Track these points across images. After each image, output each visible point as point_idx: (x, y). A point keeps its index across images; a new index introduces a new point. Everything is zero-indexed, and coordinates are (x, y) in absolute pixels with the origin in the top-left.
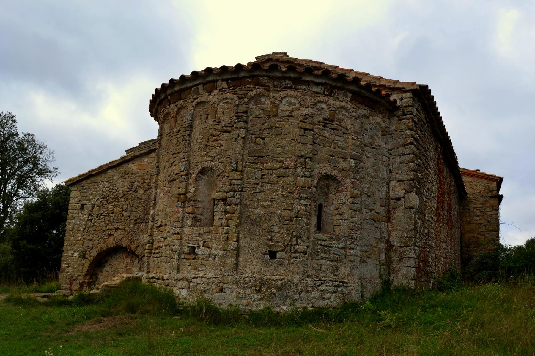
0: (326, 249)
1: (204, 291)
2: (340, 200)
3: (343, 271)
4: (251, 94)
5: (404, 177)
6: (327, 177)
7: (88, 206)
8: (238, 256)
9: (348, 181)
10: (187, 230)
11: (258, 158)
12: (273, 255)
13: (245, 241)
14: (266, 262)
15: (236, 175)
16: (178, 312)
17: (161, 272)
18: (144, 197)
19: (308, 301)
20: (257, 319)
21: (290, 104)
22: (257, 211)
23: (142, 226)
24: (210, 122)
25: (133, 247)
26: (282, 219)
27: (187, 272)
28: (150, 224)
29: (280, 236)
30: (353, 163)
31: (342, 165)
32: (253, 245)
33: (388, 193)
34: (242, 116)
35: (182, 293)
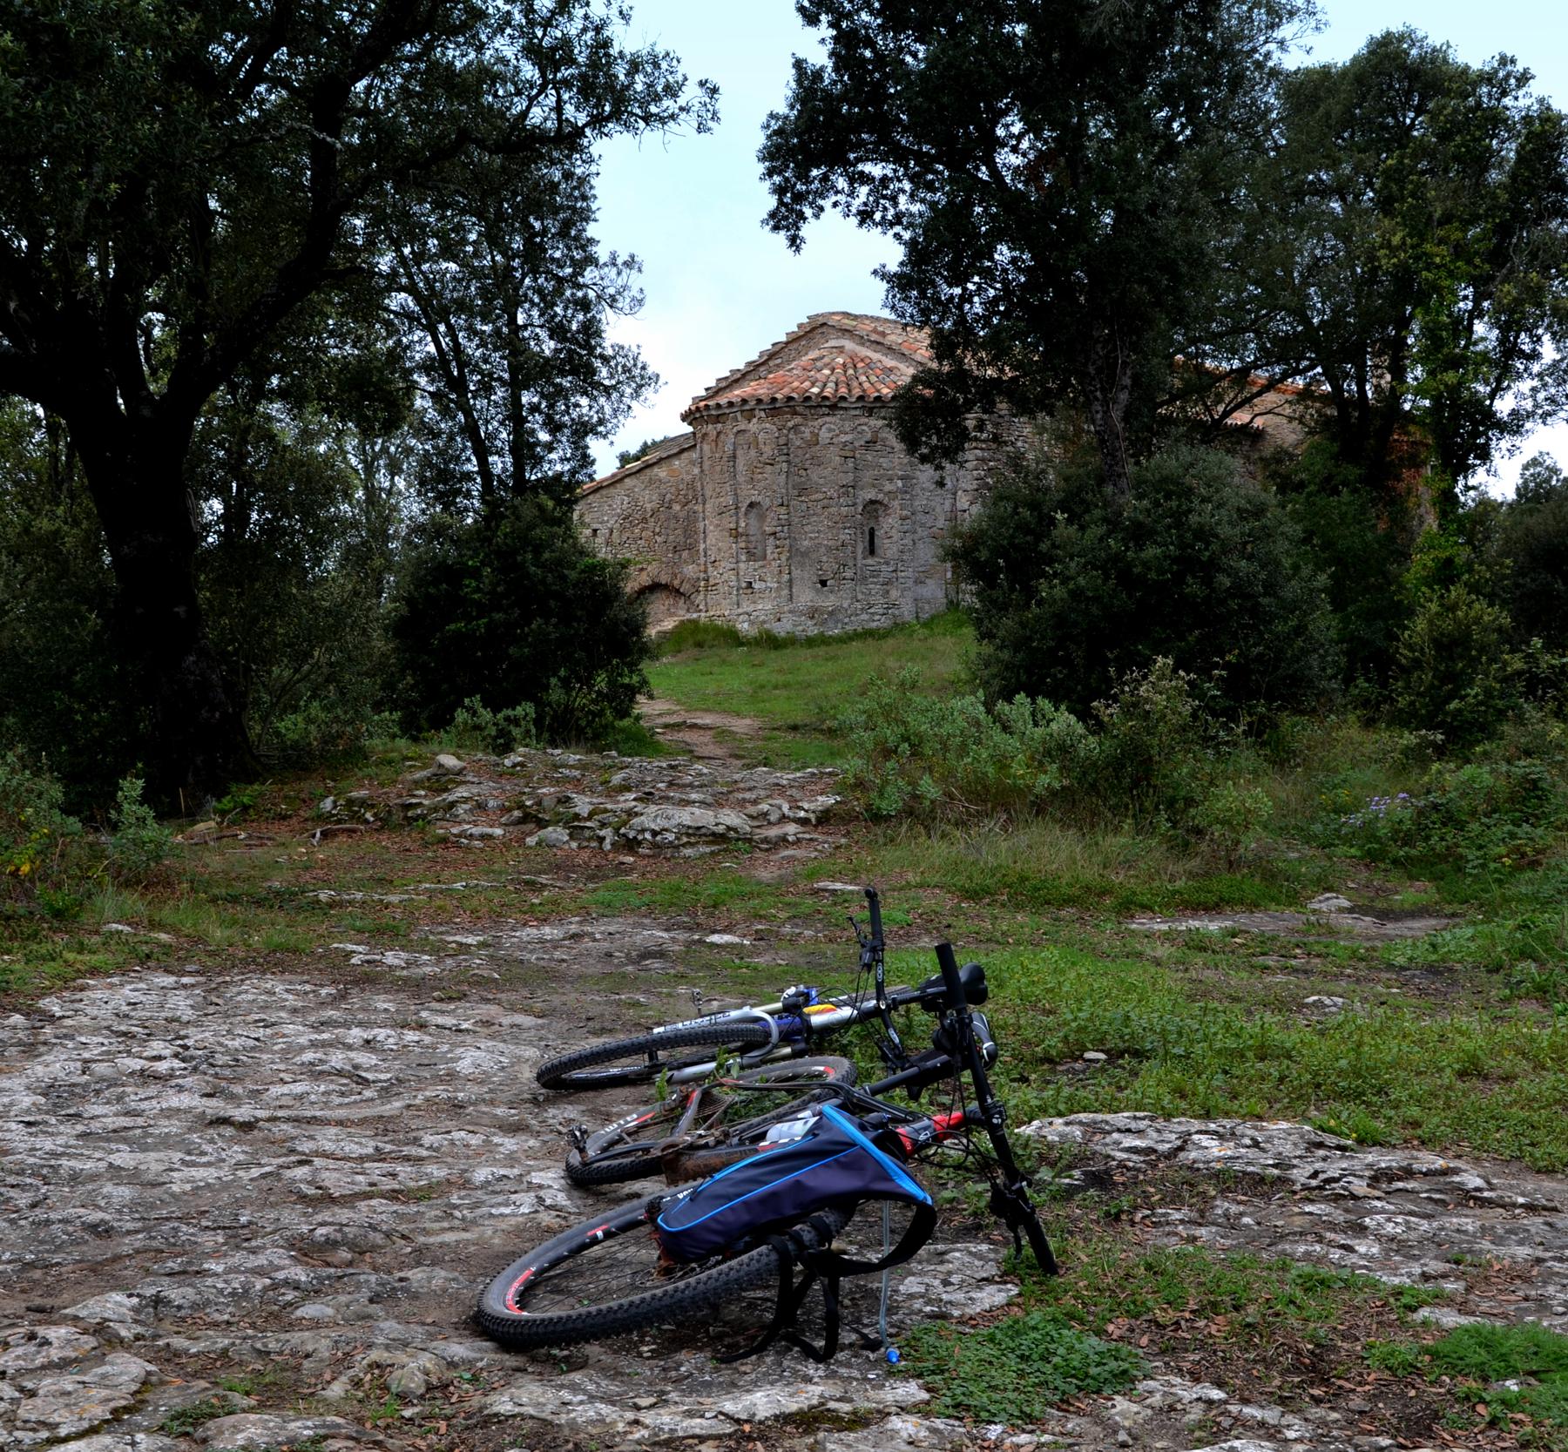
0: (876, 574)
1: (764, 622)
2: (889, 524)
3: (894, 594)
4: (790, 424)
5: (970, 487)
6: (872, 502)
7: (604, 531)
8: (791, 587)
9: (896, 503)
10: (742, 565)
11: (803, 491)
12: (824, 583)
13: (796, 573)
14: (817, 591)
15: (783, 510)
16: (742, 644)
17: (720, 608)
18: (682, 515)
19: (862, 621)
20: (810, 642)
21: (830, 430)
22: (806, 543)
23: (685, 554)
24: (753, 452)
25: (676, 583)
26: (829, 549)
27: (746, 607)
28: (702, 560)
29: (830, 566)
30: (900, 484)
31: (888, 487)
32: (805, 576)
33: (954, 505)
34: (784, 448)
35: (743, 627)
